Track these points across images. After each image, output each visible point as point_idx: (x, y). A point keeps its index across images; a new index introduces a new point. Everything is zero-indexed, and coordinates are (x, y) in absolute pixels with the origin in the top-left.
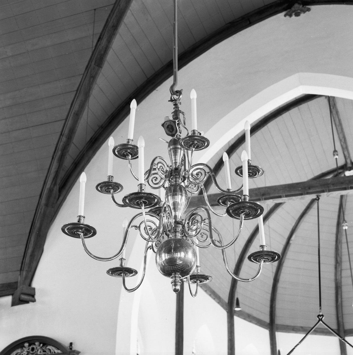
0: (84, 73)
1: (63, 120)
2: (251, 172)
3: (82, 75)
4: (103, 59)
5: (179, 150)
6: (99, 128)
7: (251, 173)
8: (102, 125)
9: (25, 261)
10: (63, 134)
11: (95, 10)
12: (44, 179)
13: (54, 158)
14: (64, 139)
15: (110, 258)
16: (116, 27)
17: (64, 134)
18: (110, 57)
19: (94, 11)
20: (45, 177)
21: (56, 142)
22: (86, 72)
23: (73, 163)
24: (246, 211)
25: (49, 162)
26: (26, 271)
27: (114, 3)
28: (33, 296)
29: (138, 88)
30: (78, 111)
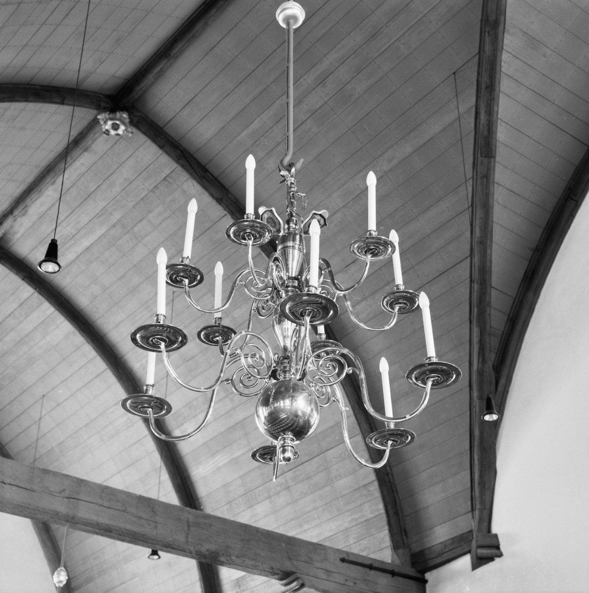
0: (473, 175)
1: (467, 257)
2: (373, 247)
3: (471, 179)
4: (490, 144)
5: (291, 250)
6: (534, 253)
7: (373, 249)
8: (537, 246)
9: (475, 494)
10: (473, 280)
11: (454, 73)
12: (467, 358)
13: (472, 321)
14: (476, 287)
15: (189, 435)
16: (492, 86)
17: (474, 279)
18: (502, 134)
19: (453, 75)
20: (468, 355)
21: (468, 295)
22: (475, 173)
23: (507, 320)
24: (308, 309)
25: (468, 331)
26: (479, 509)
27: (477, 52)
28: (497, 547)
29: (577, 167)
30: (481, 237)
